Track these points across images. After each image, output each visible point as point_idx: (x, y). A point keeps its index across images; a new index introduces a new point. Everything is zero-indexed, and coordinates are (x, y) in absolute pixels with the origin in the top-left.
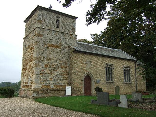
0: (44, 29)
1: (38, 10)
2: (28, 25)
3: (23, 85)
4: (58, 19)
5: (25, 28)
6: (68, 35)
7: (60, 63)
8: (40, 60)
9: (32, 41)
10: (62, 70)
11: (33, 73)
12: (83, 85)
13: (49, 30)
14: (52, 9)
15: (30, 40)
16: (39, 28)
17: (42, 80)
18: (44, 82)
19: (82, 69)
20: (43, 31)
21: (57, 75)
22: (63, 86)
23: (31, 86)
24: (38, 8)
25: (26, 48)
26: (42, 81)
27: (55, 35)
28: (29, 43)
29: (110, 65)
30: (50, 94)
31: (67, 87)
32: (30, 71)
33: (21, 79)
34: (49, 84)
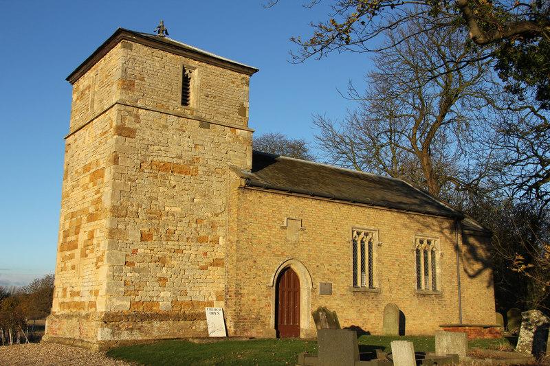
0: (141, 111)
3: (61, 300)
11: (99, 259)
15: (88, 146)
25: (76, 172)
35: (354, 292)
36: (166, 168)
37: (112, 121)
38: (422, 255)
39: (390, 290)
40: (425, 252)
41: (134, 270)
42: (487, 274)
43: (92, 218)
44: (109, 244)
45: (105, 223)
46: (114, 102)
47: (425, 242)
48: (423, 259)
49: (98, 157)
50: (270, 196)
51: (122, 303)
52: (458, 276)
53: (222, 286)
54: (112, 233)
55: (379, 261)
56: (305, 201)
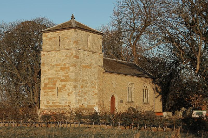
0: (80, 50)
36: (85, 67)
38: (145, 91)
40: (146, 90)
41: (80, 96)
42: (160, 97)
47: (146, 87)
48: (145, 91)
50: (109, 74)
52: (154, 99)
53: (97, 101)
56: (117, 75)
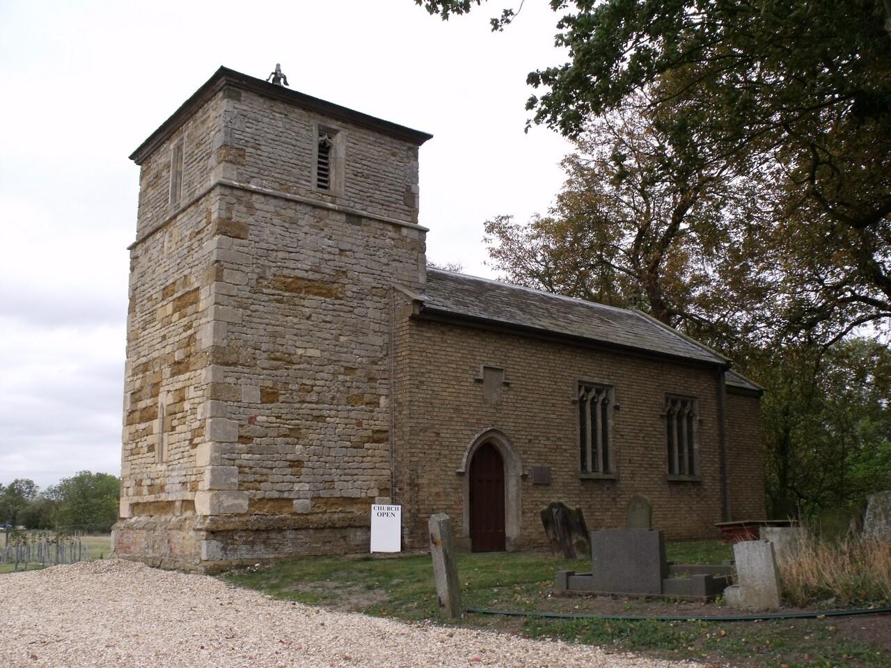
0: (255, 197)
1: (220, 94)
2: (157, 176)
3: (136, 499)
4: (325, 143)
5: (137, 189)
6: (381, 226)
7: (341, 378)
8: (235, 364)
9: (189, 260)
10: (352, 414)
11: (197, 432)
12: (465, 497)
13: (282, 203)
14: (290, 87)
15: (170, 256)
16: (228, 192)
17: (247, 470)
18: (260, 482)
19: (457, 410)
20: (250, 207)
21: (325, 443)
22: (361, 503)
23: (189, 504)
24: (222, 82)
25: (150, 299)
26: (248, 480)
27: (312, 226)
28: (164, 272)
29: (599, 392)
30: (290, 544)
31: (375, 510)
32: (175, 423)
33: (123, 467)
34: (286, 495)
35: (583, 480)
37: (210, 213)
39: (633, 477)
43: (179, 367)
44: (213, 408)
45: (204, 374)
46: (213, 182)
49: (186, 272)
51: (237, 502)
54: (217, 392)
55: (616, 431)
